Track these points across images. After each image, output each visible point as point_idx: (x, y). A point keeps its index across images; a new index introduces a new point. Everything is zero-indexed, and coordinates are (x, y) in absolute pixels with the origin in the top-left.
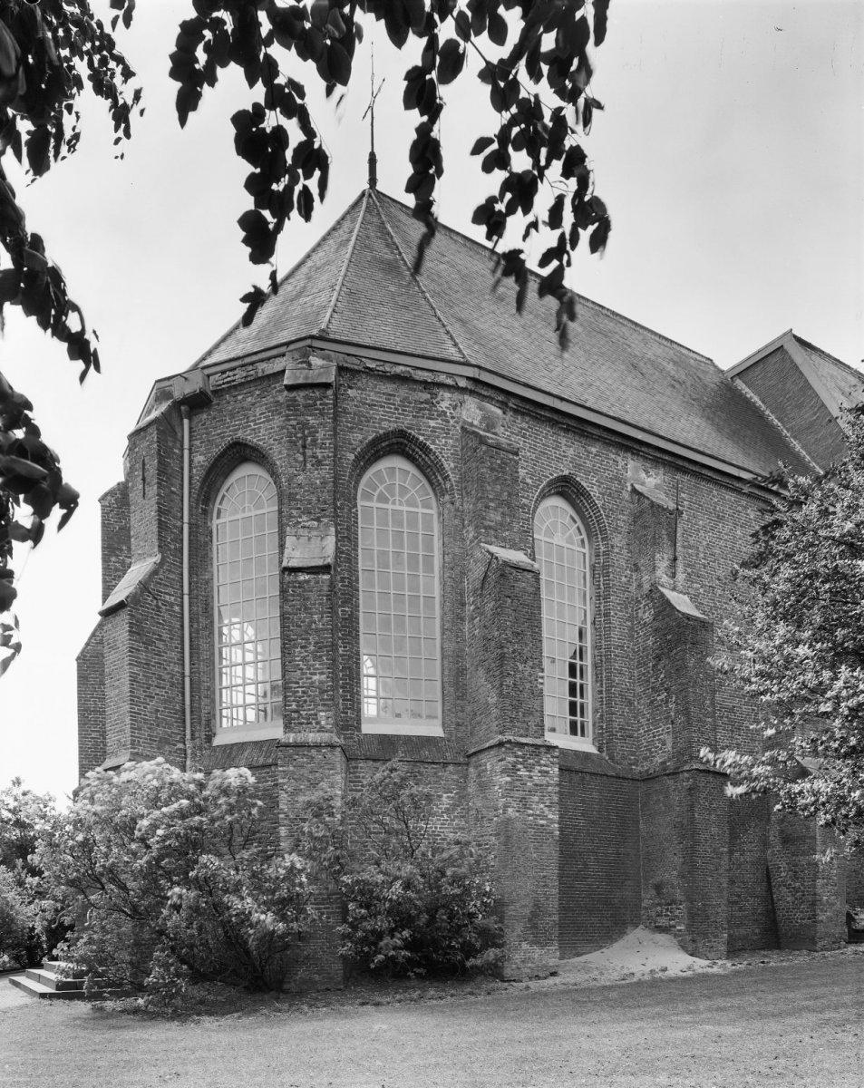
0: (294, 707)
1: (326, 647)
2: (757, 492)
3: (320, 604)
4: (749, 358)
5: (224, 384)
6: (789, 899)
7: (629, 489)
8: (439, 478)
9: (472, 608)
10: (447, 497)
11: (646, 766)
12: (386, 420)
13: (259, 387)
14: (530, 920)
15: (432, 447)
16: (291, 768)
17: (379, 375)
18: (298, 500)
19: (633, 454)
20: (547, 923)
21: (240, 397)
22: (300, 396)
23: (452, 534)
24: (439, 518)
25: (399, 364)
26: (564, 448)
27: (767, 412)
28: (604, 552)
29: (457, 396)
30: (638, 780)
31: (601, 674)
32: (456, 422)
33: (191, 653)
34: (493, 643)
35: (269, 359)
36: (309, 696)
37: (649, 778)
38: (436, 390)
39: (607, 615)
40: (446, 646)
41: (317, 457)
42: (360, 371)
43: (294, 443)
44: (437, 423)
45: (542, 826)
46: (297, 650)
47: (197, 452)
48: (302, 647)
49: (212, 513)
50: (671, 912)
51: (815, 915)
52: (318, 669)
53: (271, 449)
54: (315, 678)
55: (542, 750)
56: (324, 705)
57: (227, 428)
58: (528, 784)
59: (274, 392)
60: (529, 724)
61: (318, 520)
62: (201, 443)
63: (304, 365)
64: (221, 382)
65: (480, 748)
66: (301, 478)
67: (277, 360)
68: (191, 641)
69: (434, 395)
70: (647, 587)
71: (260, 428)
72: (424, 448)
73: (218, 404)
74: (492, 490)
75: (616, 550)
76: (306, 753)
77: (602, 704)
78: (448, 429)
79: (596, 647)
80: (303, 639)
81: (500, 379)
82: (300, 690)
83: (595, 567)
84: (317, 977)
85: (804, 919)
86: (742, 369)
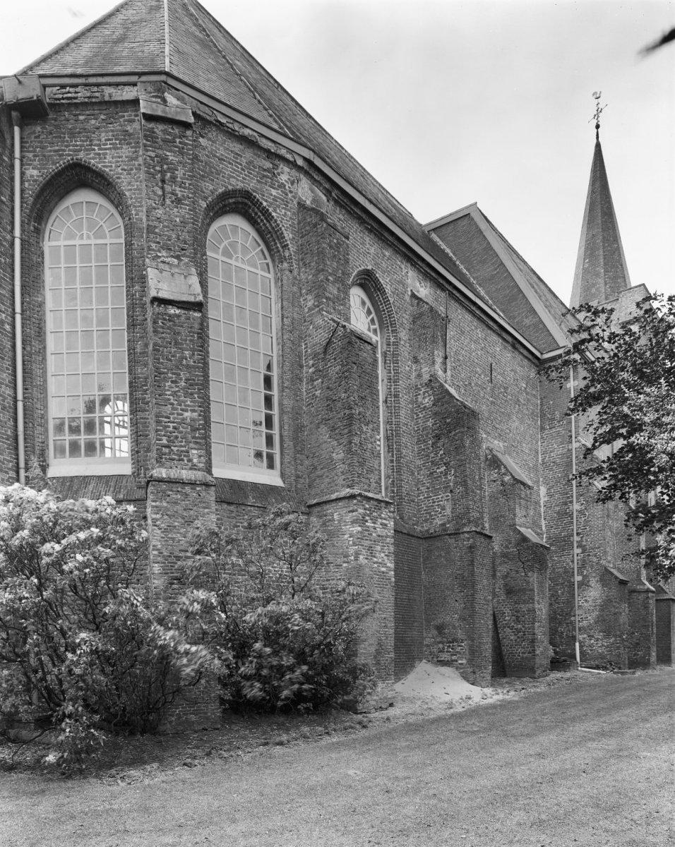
0: (165, 441)
1: (197, 384)
2: (483, 317)
3: (191, 341)
4: (442, 218)
5: (63, 99)
6: (512, 638)
7: (410, 293)
8: (278, 245)
9: (311, 370)
10: (285, 265)
11: (426, 526)
12: (234, 177)
13: (105, 112)
14: (375, 657)
15: (274, 214)
16: (165, 504)
17: (227, 132)
18: (156, 233)
19: (412, 265)
20: (387, 660)
21: (81, 118)
22: (159, 128)
23: (289, 300)
24: (276, 283)
25: (247, 127)
26: (368, 246)
27: (458, 263)
28: (393, 342)
29: (294, 172)
30: (421, 538)
31: (393, 446)
32: (293, 196)
33: (24, 377)
34: (339, 405)
35: (117, 85)
36: (181, 432)
37: (429, 537)
38: (277, 162)
39: (396, 396)
40: (285, 402)
41: (177, 195)
42: (210, 123)
43: (153, 176)
44: (277, 193)
45: (383, 573)
46: (167, 384)
47: (30, 165)
48: (172, 382)
49: (44, 233)
50: (452, 649)
51: (534, 651)
52: (189, 406)
53: (119, 178)
54: (186, 414)
55: (383, 504)
56: (196, 443)
57: (67, 146)
58: (374, 534)
59: (121, 120)
60: (371, 480)
61: (178, 257)
62: (35, 156)
63: (159, 100)
64: (61, 96)
65: (325, 499)
66: (160, 212)
67: (127, 88)
68: (24, 364)
69: (276, 167)
70: (426, 377)
71: (106, 154)
72: (266, 213)
73: (55, 120)
74: (331, 265)
75: (402, 342)
76: (179, 489)
77: (393, 472)
78: (286, 201)
79: (388, 422)
80: (173, 374)
81: (329, 169)
82: (171, 425)
83: (386, 354)
84: (193, 718)
85: (525, 653)
86: (439, 225)
